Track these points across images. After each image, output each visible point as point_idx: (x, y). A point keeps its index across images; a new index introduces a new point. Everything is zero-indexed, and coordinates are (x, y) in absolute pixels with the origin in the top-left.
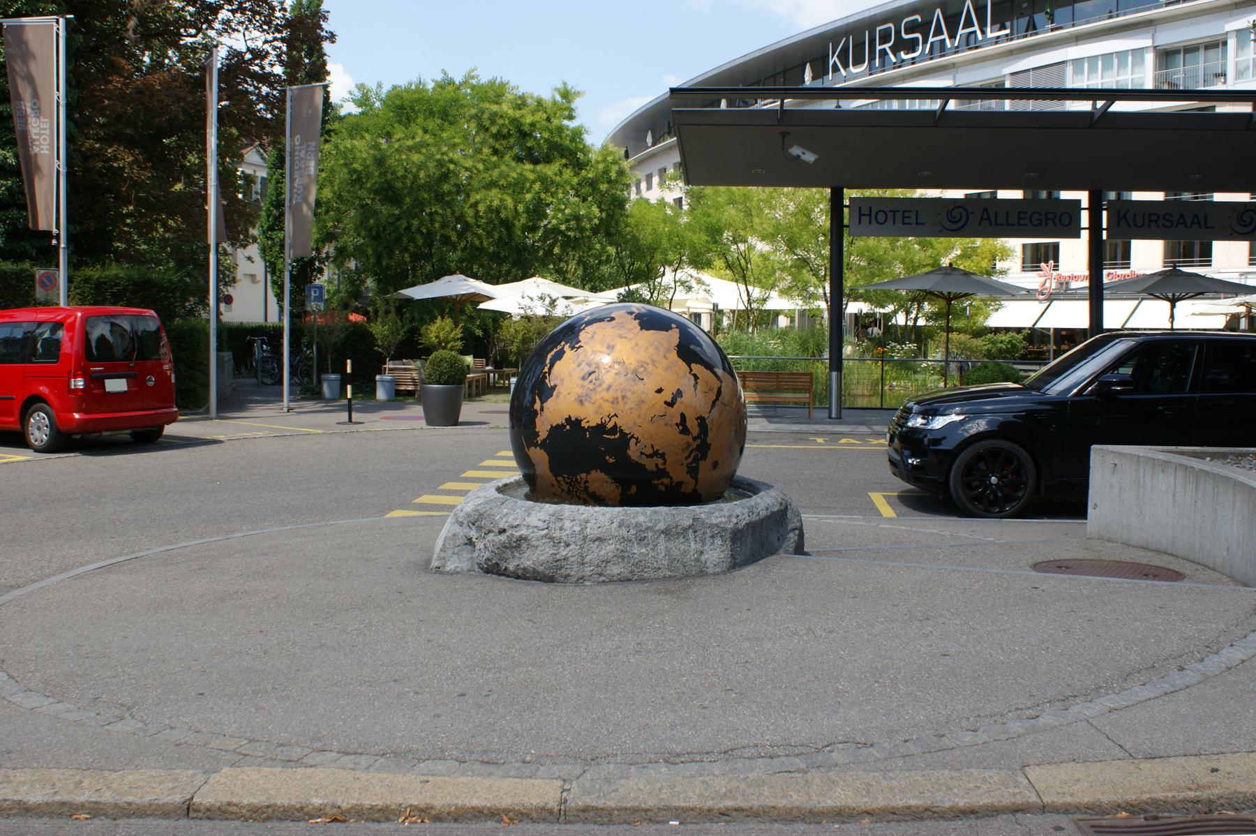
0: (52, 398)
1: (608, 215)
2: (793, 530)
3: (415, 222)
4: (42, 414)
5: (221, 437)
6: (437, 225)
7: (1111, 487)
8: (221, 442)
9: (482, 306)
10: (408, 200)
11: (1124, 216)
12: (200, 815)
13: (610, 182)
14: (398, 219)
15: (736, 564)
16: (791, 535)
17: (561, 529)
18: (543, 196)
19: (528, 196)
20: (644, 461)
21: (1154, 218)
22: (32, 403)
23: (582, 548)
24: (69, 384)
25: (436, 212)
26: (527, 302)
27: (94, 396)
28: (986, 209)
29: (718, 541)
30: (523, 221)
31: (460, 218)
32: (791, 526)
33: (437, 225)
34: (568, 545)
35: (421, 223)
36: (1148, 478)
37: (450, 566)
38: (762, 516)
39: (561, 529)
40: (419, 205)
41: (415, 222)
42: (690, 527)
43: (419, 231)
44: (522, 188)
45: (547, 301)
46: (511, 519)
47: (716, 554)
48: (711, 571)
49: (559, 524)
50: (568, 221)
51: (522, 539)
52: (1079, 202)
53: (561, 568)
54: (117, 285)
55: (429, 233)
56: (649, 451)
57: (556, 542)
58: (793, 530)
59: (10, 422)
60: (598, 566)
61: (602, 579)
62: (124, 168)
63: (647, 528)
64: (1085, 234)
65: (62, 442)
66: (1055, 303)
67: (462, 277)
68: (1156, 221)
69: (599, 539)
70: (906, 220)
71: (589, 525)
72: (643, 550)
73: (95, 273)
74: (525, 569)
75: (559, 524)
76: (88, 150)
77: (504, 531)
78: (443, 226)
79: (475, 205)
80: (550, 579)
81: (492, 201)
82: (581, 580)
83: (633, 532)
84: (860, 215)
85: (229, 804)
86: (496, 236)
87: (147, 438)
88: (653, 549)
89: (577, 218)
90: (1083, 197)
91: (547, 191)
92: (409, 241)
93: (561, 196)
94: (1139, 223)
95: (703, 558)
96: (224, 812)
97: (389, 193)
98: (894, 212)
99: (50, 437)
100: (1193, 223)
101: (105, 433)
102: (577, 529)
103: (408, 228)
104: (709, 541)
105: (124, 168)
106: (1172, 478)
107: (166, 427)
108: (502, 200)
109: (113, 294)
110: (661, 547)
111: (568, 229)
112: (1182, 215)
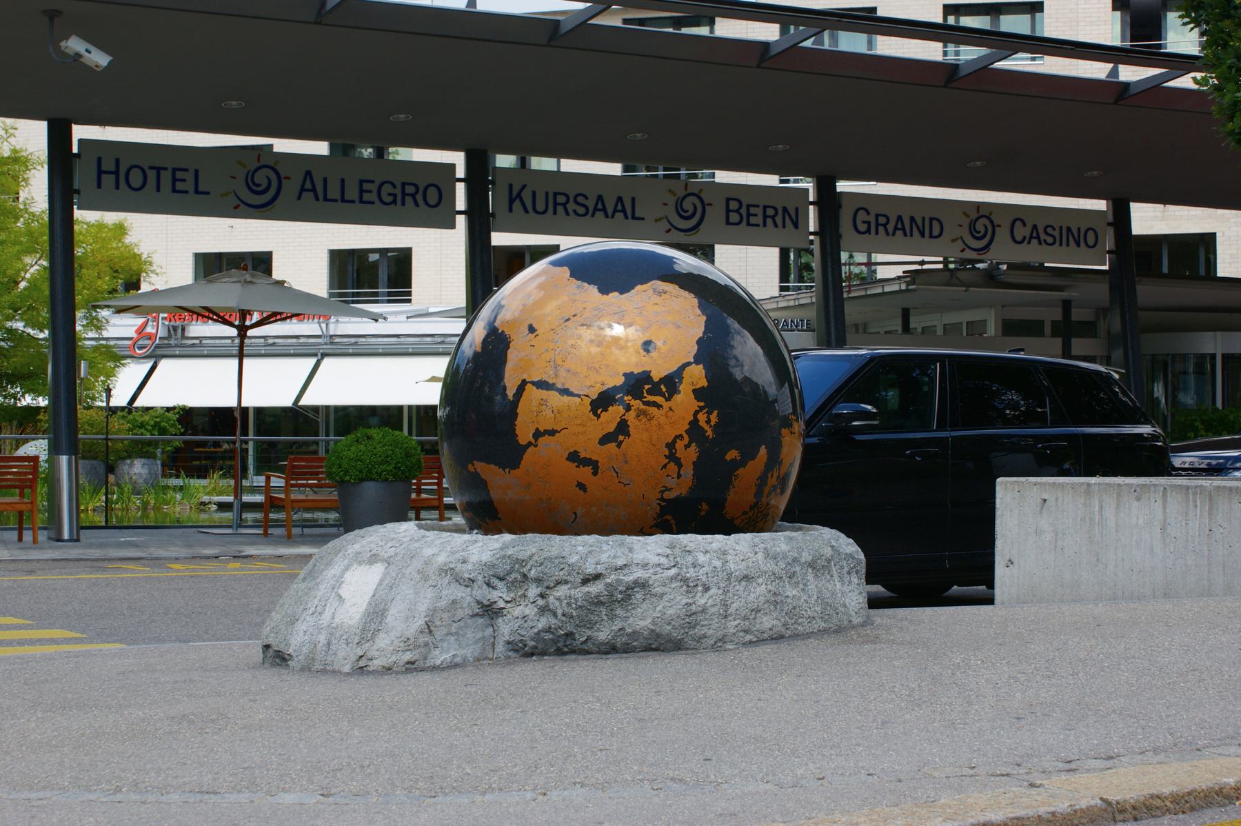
7: (1038, 532)
11: (519, 195)
12: (1127, 815)
21: (561, 199)
23: (725, 592)
28: (308, 173)
34: (707, 589)
36: (1109, 512)
37: (440, 657)
46: (604, 557)
51: (641, 585)
52: (452, 167)
57: (689, 585)
60: (746, 618)
64: (461, 221)
66: (164, 363)
68: (564, 205)
69: (746, 578)
70: (179, 186)
75: (689, 559)
77: (597, 577)
82: (719, 645)
84: (100, 172)
85: (1152, 796)
90: (457, 159)
94: (540, 206)
96: (1149, 808)
98: (158, 169)
100: (615, 211)
106: (1158, 507)
112: (600, 198)
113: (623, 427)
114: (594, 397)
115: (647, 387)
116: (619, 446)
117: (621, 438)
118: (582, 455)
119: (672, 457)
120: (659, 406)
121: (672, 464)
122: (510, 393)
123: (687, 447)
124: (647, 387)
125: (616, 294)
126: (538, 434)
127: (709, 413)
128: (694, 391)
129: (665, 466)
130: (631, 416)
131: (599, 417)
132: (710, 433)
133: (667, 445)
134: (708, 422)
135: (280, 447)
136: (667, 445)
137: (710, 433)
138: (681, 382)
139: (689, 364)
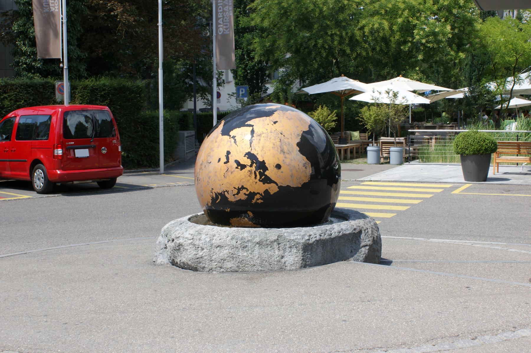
0: (45, 161)
1: (460, 30)
2: (365, 246)
3: (320, 41)
4: (40, 171)
5: (151, 185)
6: (336, 43)
8: (152, 188)
9: (354, 98)
10: (316, 26)
13: (460, 7)
14: (309, 40)
15: (305, 265)
16: (363, 249)
17: (200, 239)
18: (410, 19)
19: (400, 20)
20: (238, 197)
22: (36, 163)
24: (53, 152)
25: (335, 34)
26: (376, 95)
27: (69, 161)
29: (294, 250)
30: (397, 37)
31: (352, 38)
32: (363, 244)
33: (336, 43)
34: (203, 249)
35: (325, 42)
38: (333, 236)
39: (200, 239)
40: (325, 28)
41: (320, 41)
42: (275, 241)
43: (323, 47)
44: (396, 15)
45: (391, 94)
47: (293, 258)
48: (288, 268)
49: (199, 237)
50: (428, 36)
53: (200, 263)
54: (104, 90)
55: (330, 48)
56: (236, 191)
57: (197, 248)
58: (365, 246)
59: (24, 175)
61: (222, 270)
62: (117, 15)
63: (248, 241)
65: (52, 188)
67: (346, 78)
71: (215, 238)
72: (245, 254)
73: (90, 82)
74: (183, 263)
76: (96, 5)
78: (340, 43)
79: (362, 28)
80: (195, 269)
81: (373, 25)
83: (239, 243)
86: (378, 49)
87: (107, 185)
88: (251, 253)
89: (435, 34)
91: (413, 16)
92: (317, 54)
93: (423, 19)
95: (283, 260)
97: (305, 21)
99: (44, 184)
101: (75, 182)
102: (208, 240)
103: (316, 45)
104: (288, 250)
105: (117, 15)
107: (118, 178)
108: (380, 24)
109: (101, 96)
110: (256, 252)
111: (427, 42)
113: (243, 167)
114: (252, 152)
115: (261, 171)
116: (237, 168)
117: (239, 167)
118: (229, 156)
119: (239, 190)
120: (256, 178)
121: (237, 191)
122: (249, 123)
123: (245, 194)
124: (261, 171)
125: (298, 149)
126: (234, 137)
127: (261, 199)
128: (267, 190)
129: (235, 188)
130: (248, 168)
131: (245, 156)
132: (254, 201)
133: (242, 186)
134: (257, 199)
135: (417, 134)
136: (242, 186)
137: (254, 201)
138: (268, 183)
139: (277, 185)
